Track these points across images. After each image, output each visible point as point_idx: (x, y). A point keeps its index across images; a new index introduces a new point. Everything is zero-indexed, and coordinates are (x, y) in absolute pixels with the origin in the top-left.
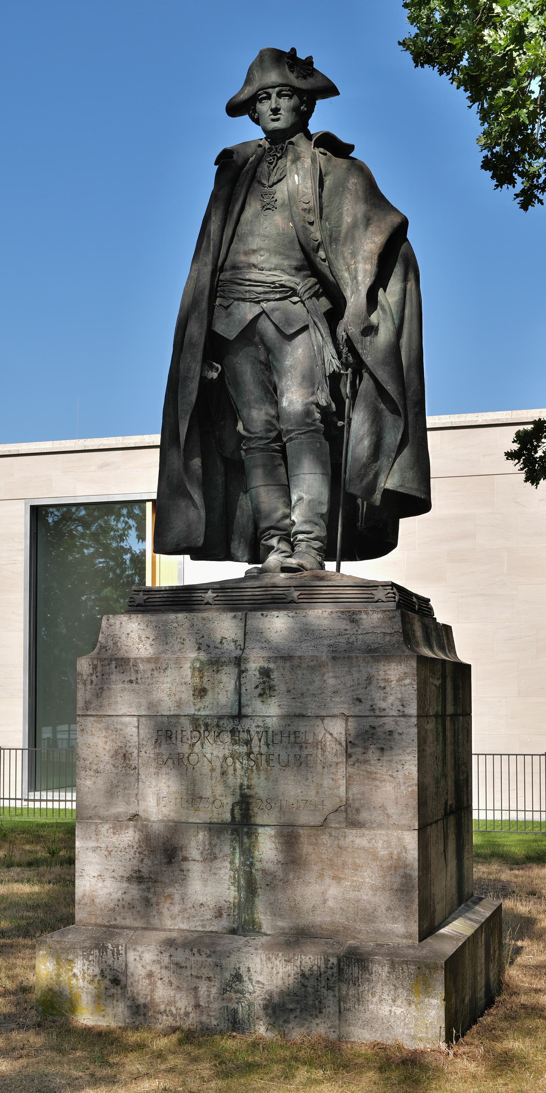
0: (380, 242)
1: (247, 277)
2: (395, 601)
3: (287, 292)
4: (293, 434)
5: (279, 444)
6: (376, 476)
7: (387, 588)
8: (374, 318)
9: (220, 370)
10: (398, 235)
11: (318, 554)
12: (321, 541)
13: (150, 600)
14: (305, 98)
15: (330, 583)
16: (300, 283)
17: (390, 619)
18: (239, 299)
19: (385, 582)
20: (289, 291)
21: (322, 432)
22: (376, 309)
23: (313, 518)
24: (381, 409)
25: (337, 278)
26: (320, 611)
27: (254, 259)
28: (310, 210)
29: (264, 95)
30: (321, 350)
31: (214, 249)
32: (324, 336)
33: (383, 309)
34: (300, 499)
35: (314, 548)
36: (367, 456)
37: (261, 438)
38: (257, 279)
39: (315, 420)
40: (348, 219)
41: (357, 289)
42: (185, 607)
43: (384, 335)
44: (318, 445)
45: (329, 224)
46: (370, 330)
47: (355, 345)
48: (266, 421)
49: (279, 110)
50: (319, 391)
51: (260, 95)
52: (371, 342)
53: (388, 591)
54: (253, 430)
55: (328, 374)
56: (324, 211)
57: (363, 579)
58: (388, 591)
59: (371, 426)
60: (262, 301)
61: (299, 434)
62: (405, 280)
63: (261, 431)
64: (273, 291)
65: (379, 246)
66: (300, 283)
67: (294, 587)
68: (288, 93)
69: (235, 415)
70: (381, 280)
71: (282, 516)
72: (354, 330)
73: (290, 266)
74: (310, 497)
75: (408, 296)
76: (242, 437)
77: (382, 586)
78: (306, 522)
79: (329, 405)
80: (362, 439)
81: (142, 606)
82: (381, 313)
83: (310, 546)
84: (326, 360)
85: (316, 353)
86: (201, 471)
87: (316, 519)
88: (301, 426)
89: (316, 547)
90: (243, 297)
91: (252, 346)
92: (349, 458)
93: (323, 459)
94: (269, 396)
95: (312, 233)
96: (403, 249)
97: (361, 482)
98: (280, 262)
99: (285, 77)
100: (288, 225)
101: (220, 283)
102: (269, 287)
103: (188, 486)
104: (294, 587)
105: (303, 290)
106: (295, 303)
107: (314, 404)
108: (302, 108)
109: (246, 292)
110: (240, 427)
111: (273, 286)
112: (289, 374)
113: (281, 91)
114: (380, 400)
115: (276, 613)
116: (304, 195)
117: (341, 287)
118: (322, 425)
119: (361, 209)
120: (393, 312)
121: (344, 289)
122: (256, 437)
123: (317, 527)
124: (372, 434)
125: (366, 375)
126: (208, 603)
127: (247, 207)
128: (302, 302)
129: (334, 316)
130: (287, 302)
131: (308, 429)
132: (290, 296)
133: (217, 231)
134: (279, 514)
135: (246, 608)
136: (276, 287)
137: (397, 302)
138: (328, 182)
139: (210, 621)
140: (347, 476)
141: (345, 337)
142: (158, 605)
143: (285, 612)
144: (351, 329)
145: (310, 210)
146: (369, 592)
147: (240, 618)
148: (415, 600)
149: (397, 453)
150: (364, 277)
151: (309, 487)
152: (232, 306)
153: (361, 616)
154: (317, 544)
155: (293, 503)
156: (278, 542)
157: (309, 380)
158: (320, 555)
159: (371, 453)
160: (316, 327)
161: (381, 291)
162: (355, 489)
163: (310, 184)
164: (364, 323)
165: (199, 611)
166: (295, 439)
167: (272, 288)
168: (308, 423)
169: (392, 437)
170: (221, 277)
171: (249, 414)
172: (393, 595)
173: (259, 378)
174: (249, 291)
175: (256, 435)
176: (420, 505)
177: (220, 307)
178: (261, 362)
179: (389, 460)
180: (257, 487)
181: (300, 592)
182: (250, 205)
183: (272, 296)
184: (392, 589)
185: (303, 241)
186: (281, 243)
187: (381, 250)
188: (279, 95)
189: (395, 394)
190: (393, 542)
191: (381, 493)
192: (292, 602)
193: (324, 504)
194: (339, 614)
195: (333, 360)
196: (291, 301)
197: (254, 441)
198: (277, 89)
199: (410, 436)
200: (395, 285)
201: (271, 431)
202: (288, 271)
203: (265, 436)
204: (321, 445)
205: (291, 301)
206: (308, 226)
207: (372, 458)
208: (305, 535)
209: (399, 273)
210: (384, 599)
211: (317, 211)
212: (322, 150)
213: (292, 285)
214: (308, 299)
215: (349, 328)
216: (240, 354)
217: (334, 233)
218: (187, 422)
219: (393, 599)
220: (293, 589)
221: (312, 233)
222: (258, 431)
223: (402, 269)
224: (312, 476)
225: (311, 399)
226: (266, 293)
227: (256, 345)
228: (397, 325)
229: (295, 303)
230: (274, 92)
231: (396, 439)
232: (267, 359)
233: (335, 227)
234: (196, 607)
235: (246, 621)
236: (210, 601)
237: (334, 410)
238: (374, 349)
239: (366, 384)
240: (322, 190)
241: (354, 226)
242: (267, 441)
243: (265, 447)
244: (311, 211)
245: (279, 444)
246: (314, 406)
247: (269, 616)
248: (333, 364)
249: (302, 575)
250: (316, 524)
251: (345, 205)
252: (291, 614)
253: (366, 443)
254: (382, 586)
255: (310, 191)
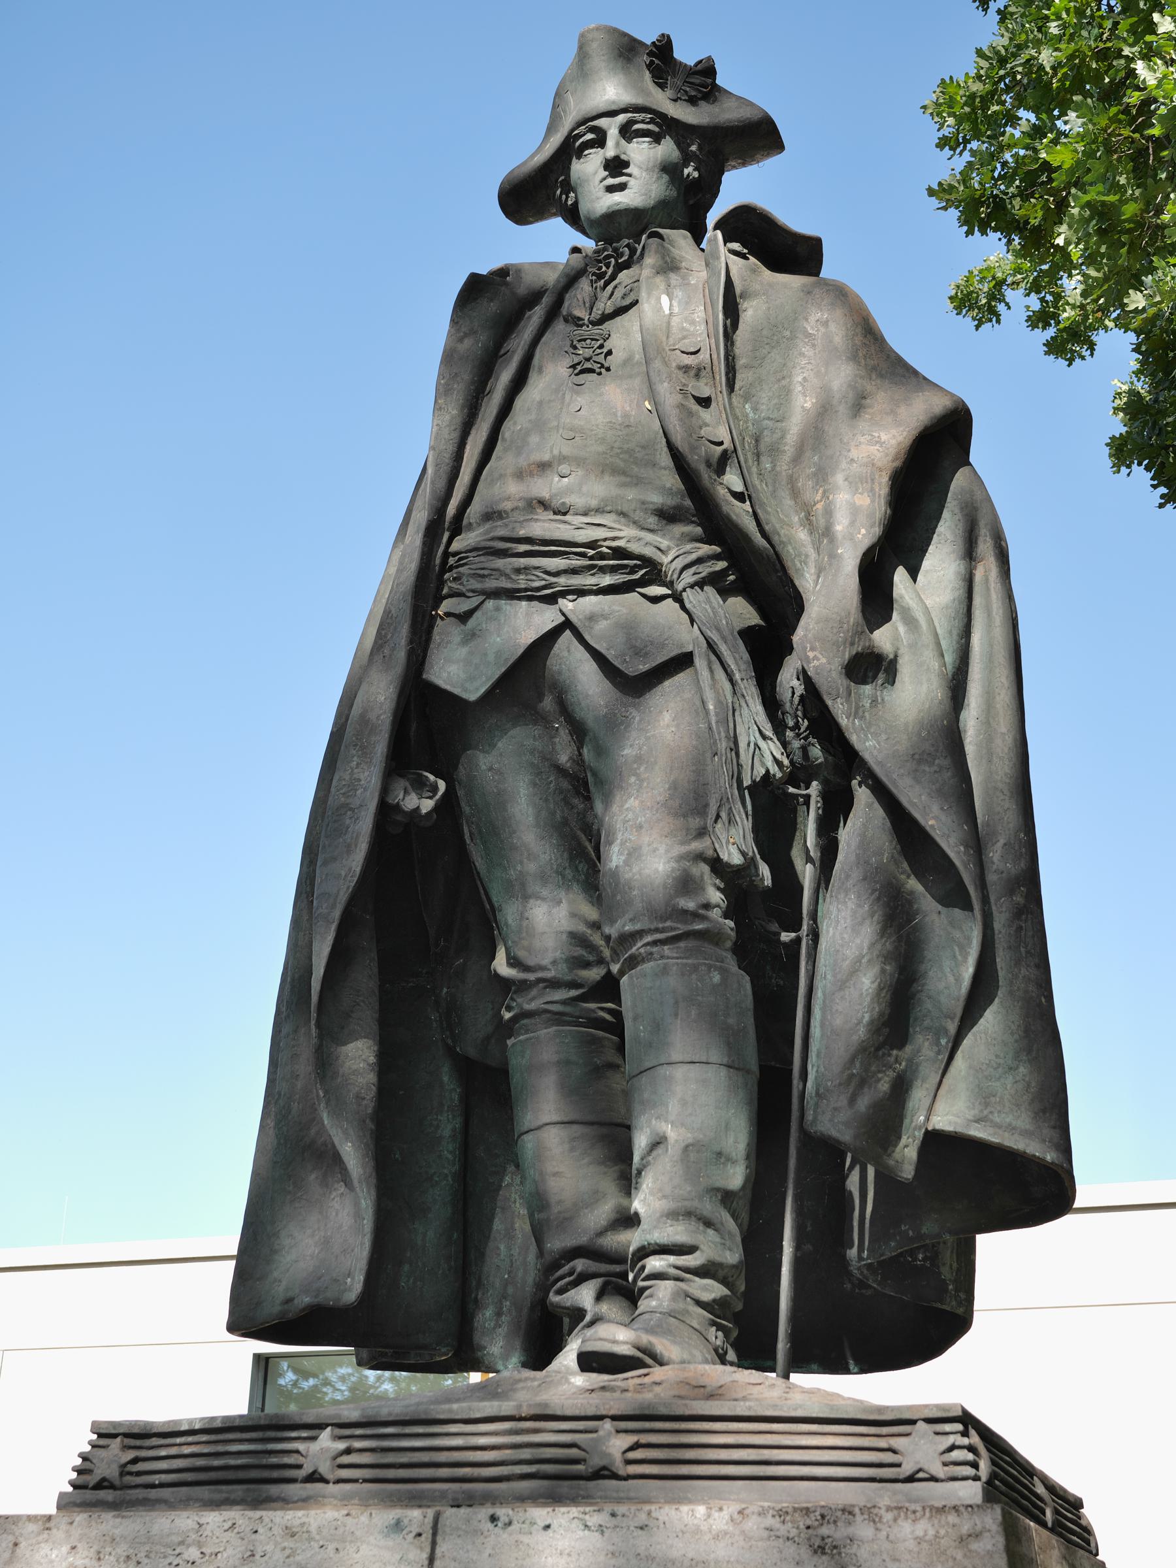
0: (894, 442)
1: (522, 533)
2: (976, 1478)
3: (633, 570)
4: (639, 944)
5: (610, 1005)
6: (901, 1088)
7: (948, 1427)
8: (883, 638)
9: (440, 793)
10: (943, 443)
11: (713, 1324)
12: (724, 1282)
13: (141, 1466)
14: (694, 148)
15: (741, 1409)
16: (669, 548)
17: (962, 1540)
18: (497, 594)
19: (938, 1407)
20: (640, 567)
21: (729, 944)
22: (888, 618)
23: (696, 1203)
24: (912, 893)
25: (775, 539)
26: (701, 1510)
27: (544, 487)
28: (699, 370)
29: (589, 136)
30: (729, 714)
31: (436, 472)
32: (737, 676)
33: (910, 621)
34: (658, 1143)
35: (698, 1303)
36: (872, 1022)
37: (554, 984)
38: (548, 536)
39: (707, 906)
40: (804, 403)
41: (833, 556)
42: (238, 1490)
43: (914, 693)
44: (716, 978)
45: (755, 409)
46: (869, 667)
47: (829, 703)
48: (572, 935)
49: (626, 164)
50: (719, 825)
51: (580, 136)
52: (874, 702)
53: (951, 1439)
54: (531, 962)
55: (747, 782)
56: (739, 376)
57: (861, 1402)
58: (951, 1439)
59: (883, 933)
60: (563, 594)
61: (655, 943)
62: (970, 553)
63: (554, 962)
64: (592, 567)
65: (892, 451)
66: (669, 548)
67: (614, 1418)
68: (651, 127)
69: (485, 929)
70: (898, 543)
71: (613, 1216)
72: (824, 660)
73: (643, 503)
74: (689, 1137)
75: (978, 600)
76: (505, 986)
77: (929, 1421)
78: (673, 1215)
79: (750, 863)
80: (854, 972)
81: (112, 1487)
82: (902, 629)
83: (687, 1295)
84: (742, 745)
85: (713, 719)
86: (372, 1078)
87: (709, 1207)
88: (663, 919)
89: (707, 1297)
90: (509, 585)
91: (535, 723)
92: (816, 1031)
93: (731, 1021)
94: (583, 867)
95: (707, 425)
96: (960, 480)
97: (852, 1101)
98: (615, 491)
99: (643, 91)
100: (640, 405)
101: (451, 561)
102: (583, 555)
103: (325, 1116)
104: (614, 1418)
105: (679, 564)
106: (655, 600)
107: (705, 860)
108: (686, 171)
109: (518, 571)
110: (501, 965)
111: (591, 552)
112: (633, 779)
113: (631, 122)
114: (905, 865)
115: (540, 1514)
116: (684, 338)
117: (788, 564)
118: (731, 924)
119: (842, 376)
120: (939, 631)
121: (797, 570)
122: (539, 980)
123: (710, 1232)
124: (886, 958)
125: (862, 795)
126: (315, 1477)
127: (533, 377)
128: (678, 598)
129: (768, 646)
130: (633, 597)
131: (682, 928)
132: (643, 582)
133: (446, 431)
134: (603, 1212)
135: (443, 1495)
136: (602, 557)
137: (947, 607)
138: (750, 312)
139: (310, 1539)
140: (809, 1084)
141: (800, 689)
142: (162, 1485)
143: (574, 1511)
144: (815, 658)
145: (699, 370)
146: (882, 1443)
147: (415, 1530)
148: (1040, 1489)
149: (962, 1019)
150: (852, 523)
151: (689, 1112)
152: (478, 614)
153: (850, 1530)
154: (711, 1290)
155: (636, 1158)
156: (599, 1297)
157: (694, 808)
158: (720, 1328)
159: (881, 1014)
160: (713, 658)
161: (900, 576)
162: (833, 1117)
163: (702, 314)
164: (852, 644)
165: (285, 1502)
166: (643, 961)
167: (591, 558)
168: (685, 912)
169: (951, 972)
170: (456, 546)
171: (522, 917)
172: (970, 1457)
173: (553, 814)
174: (526, 570)
175: (540, 975)
176: (1037, 1190)
177: (448, 620)
178: (560, 770)
179: (938, 1043)
180: (539, 1128)
181: (631, 1439)
182: (540, 370)
183: (588, 580)
184: (965, 1434)
185: (678, 439)
186: (617, 445)
187: (898, 464)
188: (626, 132)
189: (952, 840)
190: (960, 1311)
191: (918, 1142)
192: (604, 1473)
193: (734, 1162)
194: (770, 1521)
195: (761, 743)
196: (644, 596)
197: (534, 992)
198: (622, 118)
199: (1001, 974)
200: (941, 563)
201: (587, 965)
202: (638, 515)
203: (568, 978)
204: (724, 980)
205: (644, 596)
206: (695, 407)
207: (886, 1031)
208: (672, 1259)
209: (950, 536)
210: (939, 1471)
211: (721, 368)
212: (736, 246)
213: (648, 552)
214: (692, 587)
215: (811, 654)
216: (500, 745)
217: (766, 432)
218: (334, 927)
219: (968, 1471)
220: (608, 1425)
221: (707, 425)
222: (546, 962)
223: (961, 526)
224: (694, 1071)
225: (696, 846)
226: (574, 571)
227: (540, 719)
228: (950, 668)
229: (655, 600)
230: (612, 127)
231: (958, 980)
232: (579, 760)
233: (769, 419)
234: (274, 1490)
235: (434, 1544)
236: (325, 1469)
237: (768, 882)
238: (887, 723)
239: (864, 821)
240: (735, 325)
241: (824, 410)
242: (574, 993)
243: (568, 1009)
244: (703, 373)
245: (610, 1005)
246: (706, 868)
247: (515, 1526)
248: (767, 755)
249: (646, 1380)
250: (708, 1223)
251: (798, 370)
252: (594, 1519)
253: (867, 982)
254: (929, 1421)
255: (702, 328)
